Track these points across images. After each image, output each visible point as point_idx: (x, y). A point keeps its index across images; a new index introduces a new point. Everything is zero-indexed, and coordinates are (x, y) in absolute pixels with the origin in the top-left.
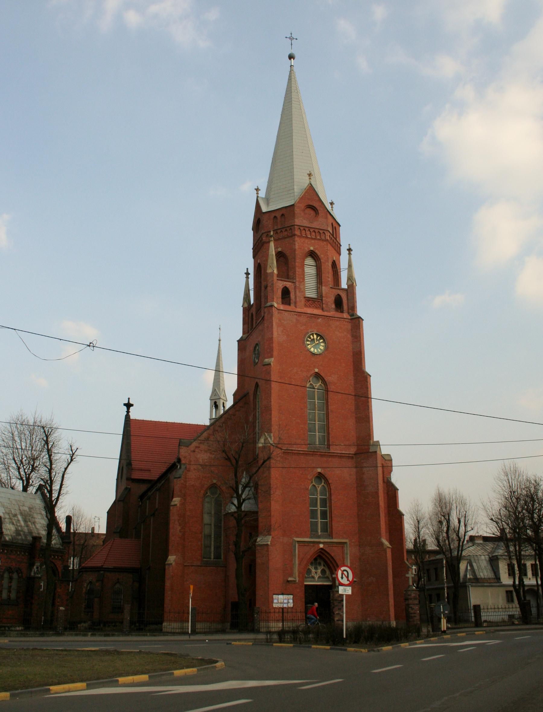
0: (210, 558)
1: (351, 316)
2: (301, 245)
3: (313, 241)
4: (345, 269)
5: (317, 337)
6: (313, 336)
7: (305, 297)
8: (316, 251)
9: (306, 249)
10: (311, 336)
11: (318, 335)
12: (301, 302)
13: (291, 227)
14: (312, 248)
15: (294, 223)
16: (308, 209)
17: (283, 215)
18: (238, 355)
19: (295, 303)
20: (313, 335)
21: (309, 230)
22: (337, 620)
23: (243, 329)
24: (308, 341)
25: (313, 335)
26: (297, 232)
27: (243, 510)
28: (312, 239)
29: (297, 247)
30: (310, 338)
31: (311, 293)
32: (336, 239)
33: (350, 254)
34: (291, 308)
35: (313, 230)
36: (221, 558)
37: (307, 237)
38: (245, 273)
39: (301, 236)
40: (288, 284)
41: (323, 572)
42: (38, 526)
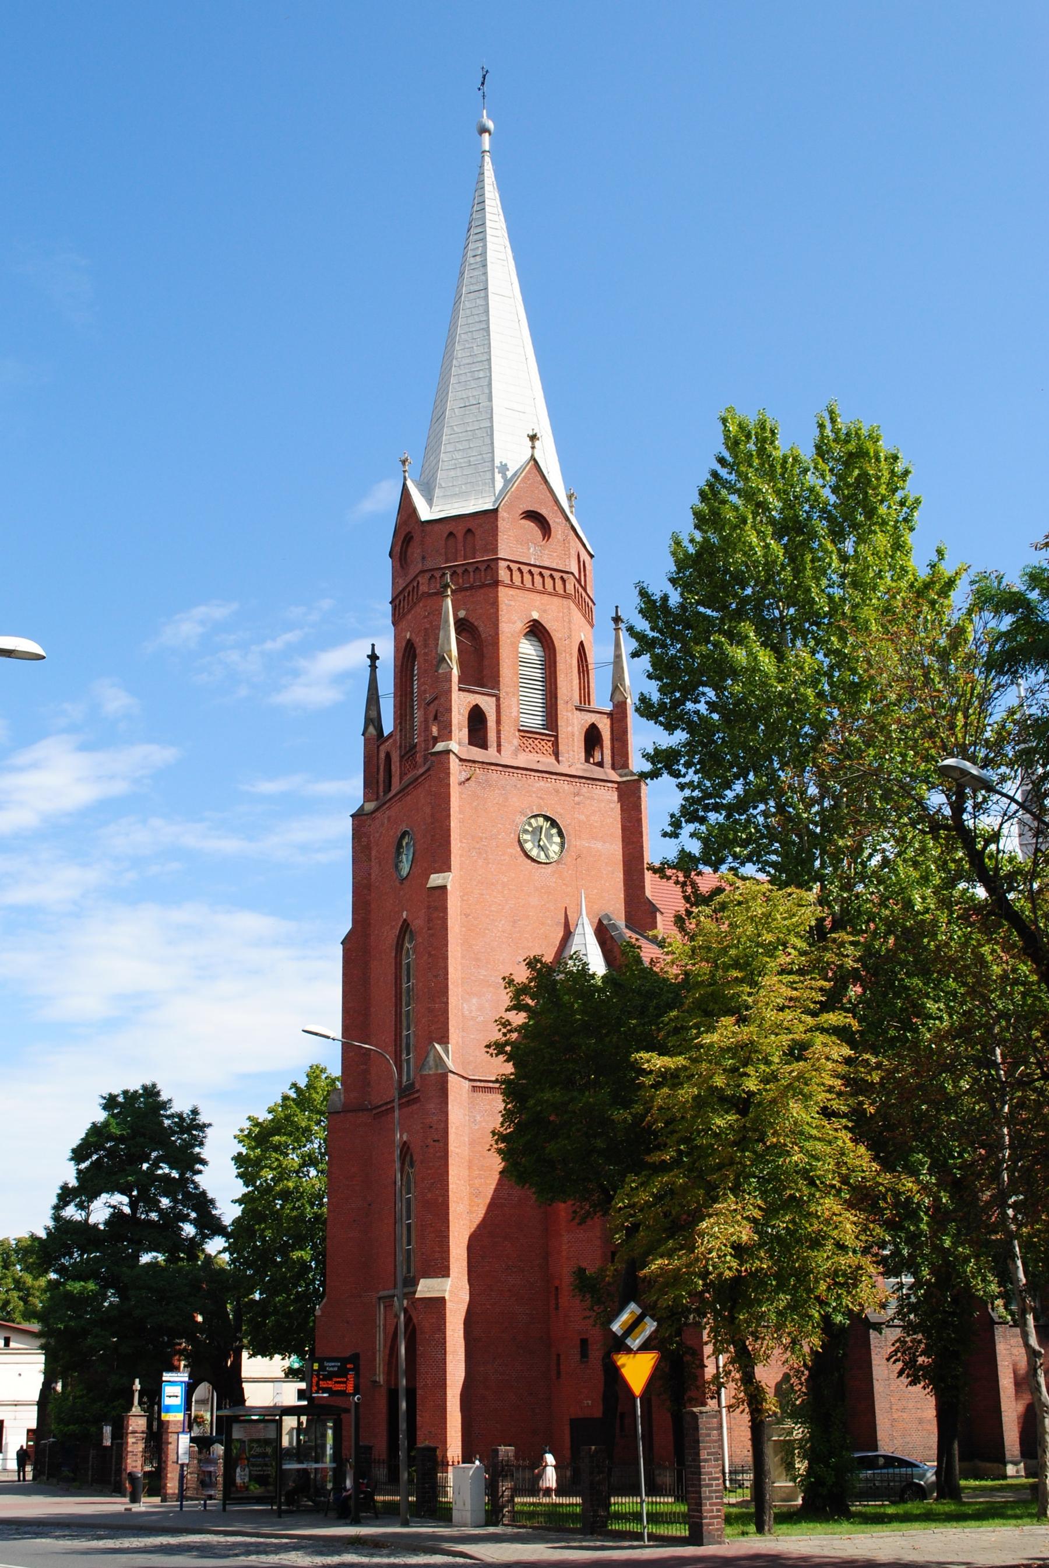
2: (515, 608)
4: (602, 665)
12: (511, 740)
13: (491, 566)
14: (535, 616)
15: (495, 550)
18: (344, 974)
19: (499, 745)
26: (503, 575)
27: (655, 1324)
32: (585, 590)
34: (490, 754)
38: (368, 656)
39: (512, 586)
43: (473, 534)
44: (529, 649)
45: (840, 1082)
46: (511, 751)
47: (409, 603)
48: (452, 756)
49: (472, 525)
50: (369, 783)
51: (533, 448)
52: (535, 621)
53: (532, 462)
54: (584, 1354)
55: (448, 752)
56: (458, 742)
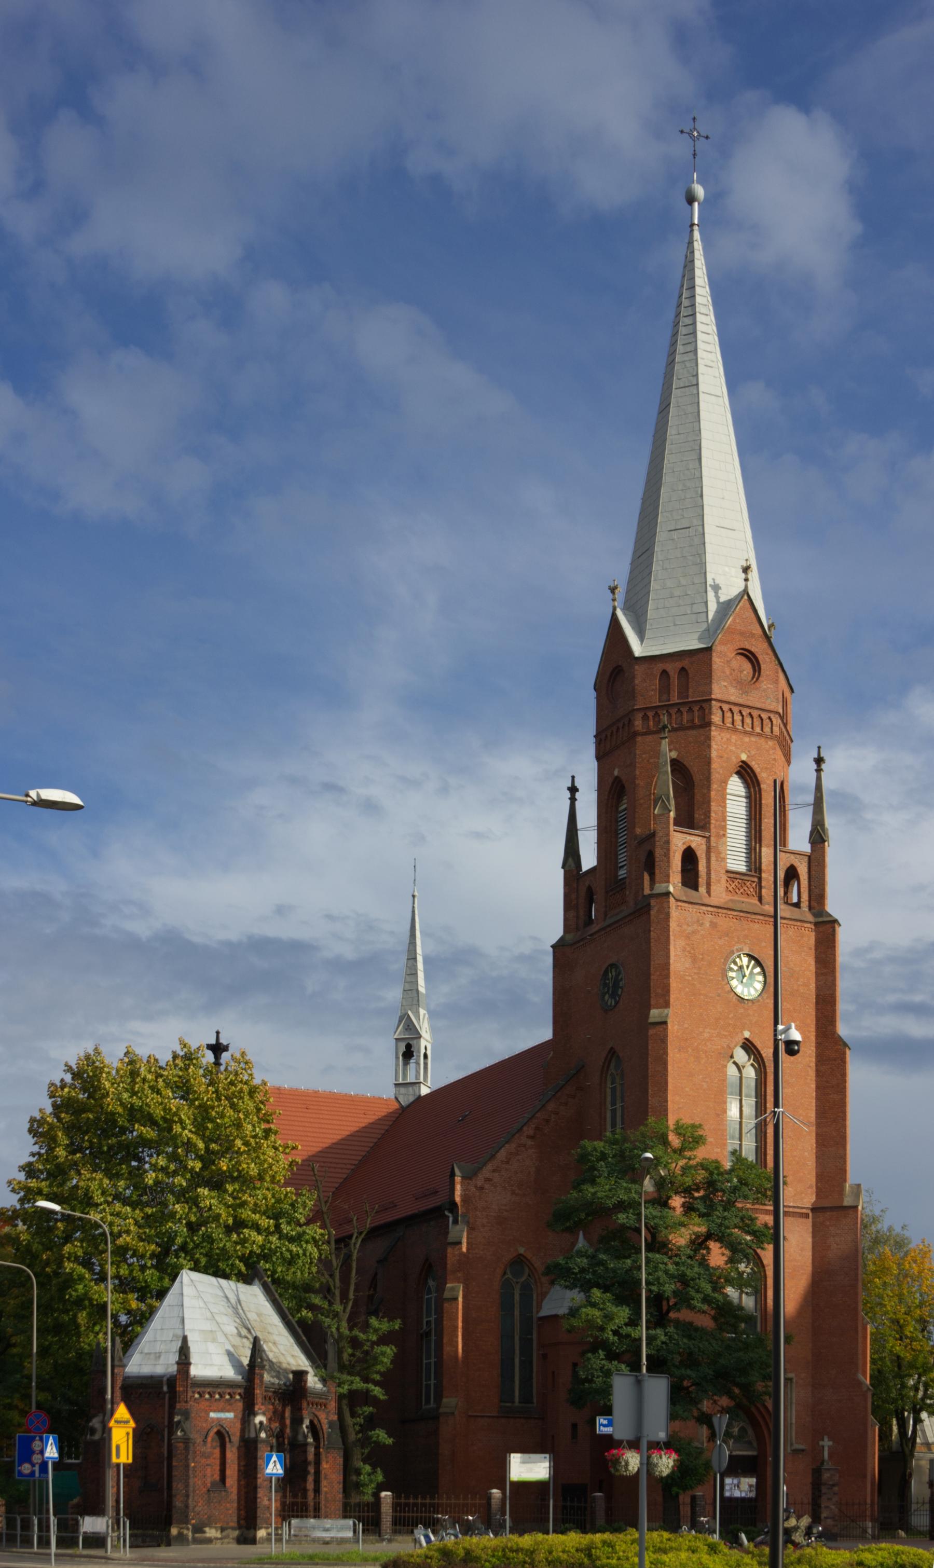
0: (513, 1402)
1: (815, 915)
2: (726, 746)
3: (747, 739)
5: (749, 962)
6: (741, 959)
7: (727, 872)
8: (753, 764)
9: (733, 758)
10: (738, 960)
11: (751, 957)
13: (704, 704)
14: (744, 757)
15: (710, 693)
16: (739, 657)
17: (683, 669)
19: (708, 885)
20: (739, 956)
21: (740, 712)
22: (825, 1518)
23: (566, 920)
24: (731, 970)
25: (739, 956)
26: (716, 718)
28: (746, 733)
29: (714, 754)
30: (735, 963)
31: (737, 862)
33: (819, 771)
35: (749, 711)
36: (533, 1403)
37: (735, 730)
38: (569, 789)
39: (723, 727)
40: (696, 841)
41: (742, 1430)
42: (282, 1348)
43: (687, 674)
44: (736, 786)
45: (695, 1303)
46: (720, 893)
47: (615, 740)
48: (672, 899)
49: (685, 663)
50: (817, 1196)
51: (746, 580)
52: (743, 762)
53: (746, 597)
54: (574, 1435)
55: (668, 894)
56: (674, 885)
